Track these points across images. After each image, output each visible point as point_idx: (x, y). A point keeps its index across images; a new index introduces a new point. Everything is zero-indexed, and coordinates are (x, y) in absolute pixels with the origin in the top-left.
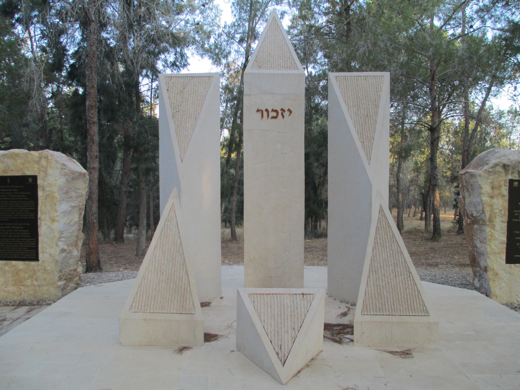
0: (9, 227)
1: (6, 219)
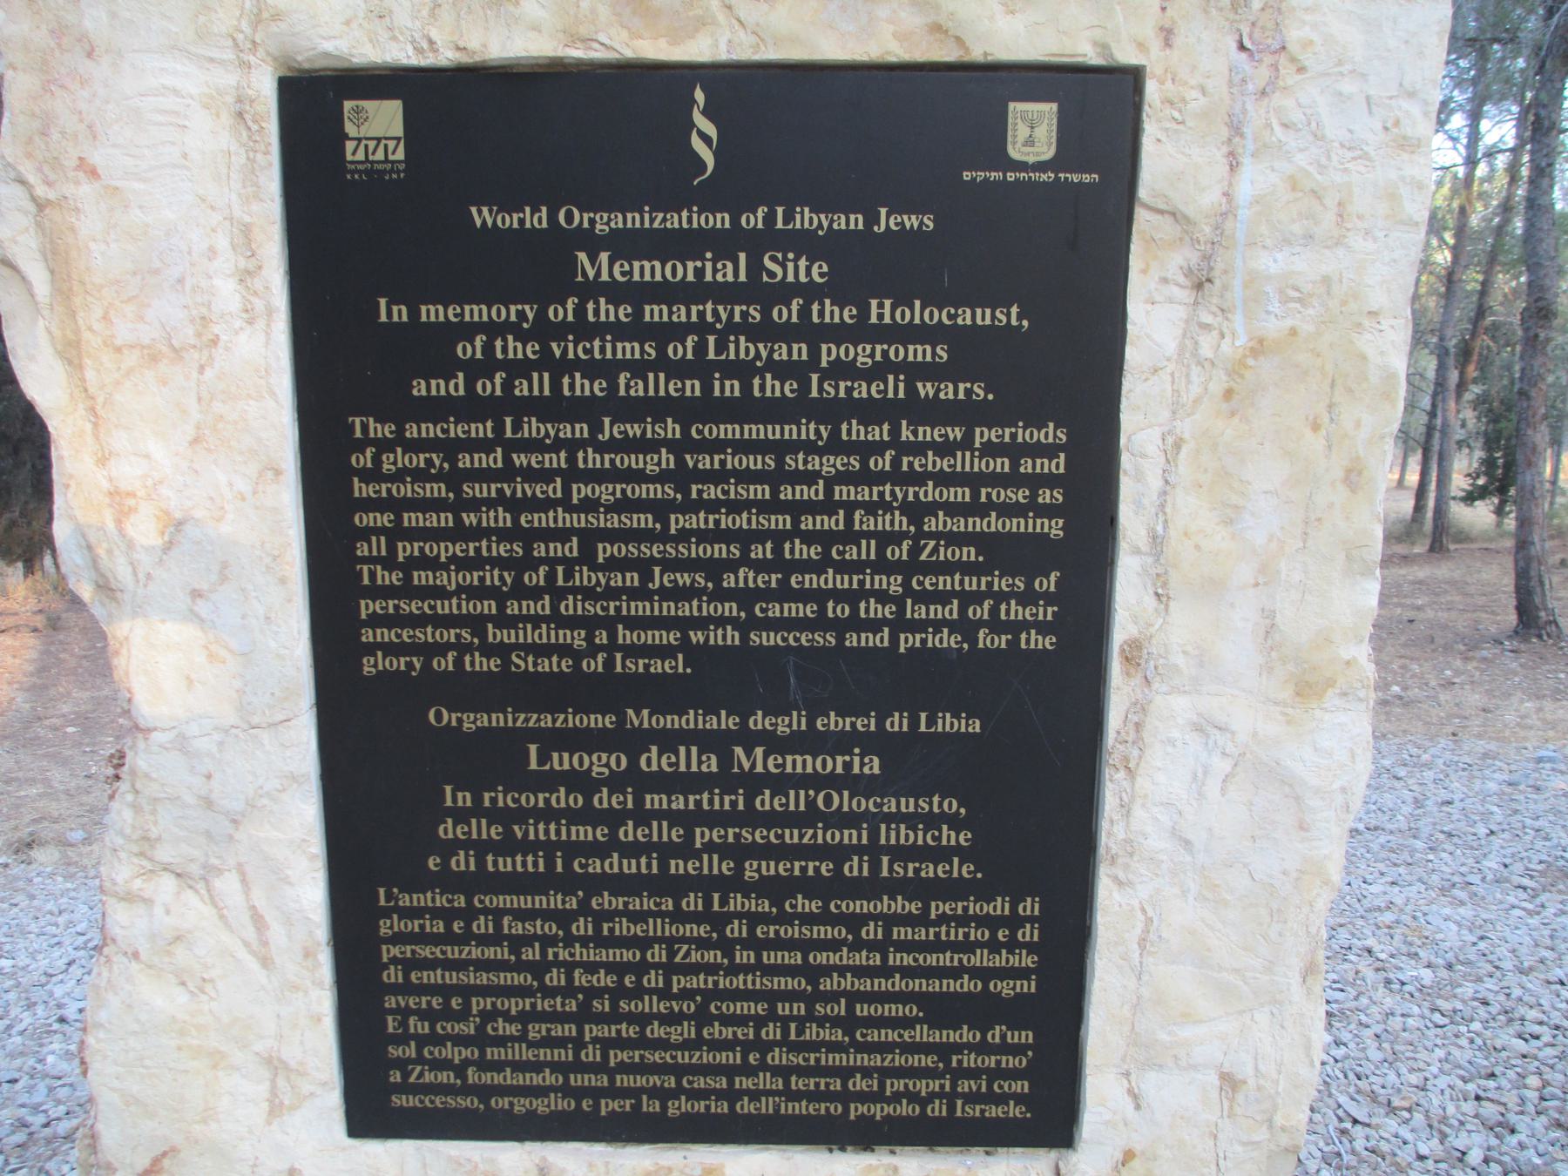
0: (690, 759)
1: (665, 652)
